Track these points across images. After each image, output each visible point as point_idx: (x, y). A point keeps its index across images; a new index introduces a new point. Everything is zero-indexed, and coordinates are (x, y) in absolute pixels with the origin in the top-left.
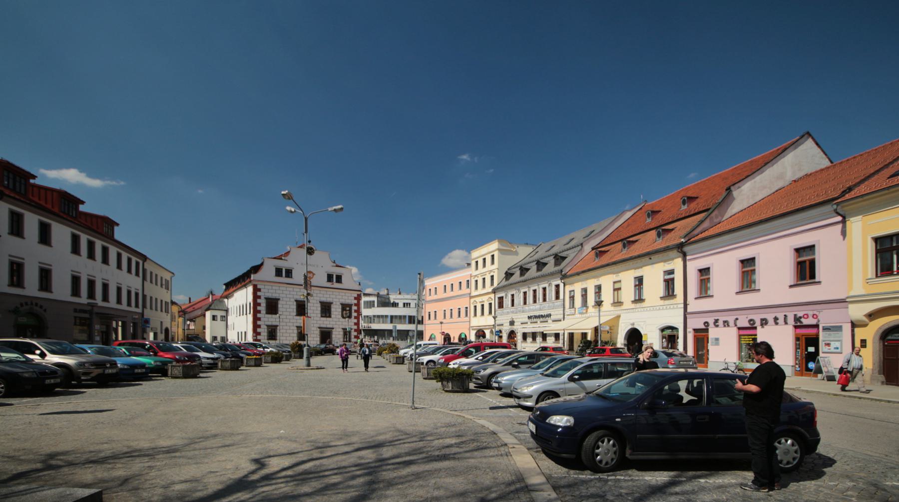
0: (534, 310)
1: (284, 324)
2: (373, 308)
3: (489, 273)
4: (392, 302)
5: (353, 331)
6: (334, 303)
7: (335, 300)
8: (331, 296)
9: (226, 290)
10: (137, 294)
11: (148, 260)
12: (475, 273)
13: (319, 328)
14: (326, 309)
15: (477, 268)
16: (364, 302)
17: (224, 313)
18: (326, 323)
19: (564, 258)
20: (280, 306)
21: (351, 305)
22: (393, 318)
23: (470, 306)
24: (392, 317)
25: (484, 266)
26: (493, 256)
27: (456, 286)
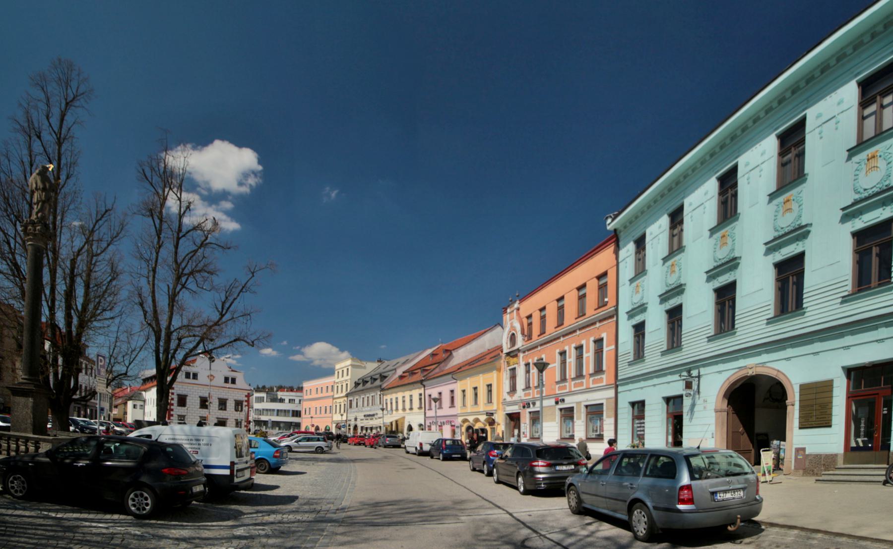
2: (262, 403)
7: (230, 397)
9: (142, 384)
14: (223, 404)
16: (256, 398)
17: (142, 403)
19: (385, 377)
22: (279, 412)
24: (278, 411)
25: (343, 376)
26: (348, 369)
27: (325, 389)
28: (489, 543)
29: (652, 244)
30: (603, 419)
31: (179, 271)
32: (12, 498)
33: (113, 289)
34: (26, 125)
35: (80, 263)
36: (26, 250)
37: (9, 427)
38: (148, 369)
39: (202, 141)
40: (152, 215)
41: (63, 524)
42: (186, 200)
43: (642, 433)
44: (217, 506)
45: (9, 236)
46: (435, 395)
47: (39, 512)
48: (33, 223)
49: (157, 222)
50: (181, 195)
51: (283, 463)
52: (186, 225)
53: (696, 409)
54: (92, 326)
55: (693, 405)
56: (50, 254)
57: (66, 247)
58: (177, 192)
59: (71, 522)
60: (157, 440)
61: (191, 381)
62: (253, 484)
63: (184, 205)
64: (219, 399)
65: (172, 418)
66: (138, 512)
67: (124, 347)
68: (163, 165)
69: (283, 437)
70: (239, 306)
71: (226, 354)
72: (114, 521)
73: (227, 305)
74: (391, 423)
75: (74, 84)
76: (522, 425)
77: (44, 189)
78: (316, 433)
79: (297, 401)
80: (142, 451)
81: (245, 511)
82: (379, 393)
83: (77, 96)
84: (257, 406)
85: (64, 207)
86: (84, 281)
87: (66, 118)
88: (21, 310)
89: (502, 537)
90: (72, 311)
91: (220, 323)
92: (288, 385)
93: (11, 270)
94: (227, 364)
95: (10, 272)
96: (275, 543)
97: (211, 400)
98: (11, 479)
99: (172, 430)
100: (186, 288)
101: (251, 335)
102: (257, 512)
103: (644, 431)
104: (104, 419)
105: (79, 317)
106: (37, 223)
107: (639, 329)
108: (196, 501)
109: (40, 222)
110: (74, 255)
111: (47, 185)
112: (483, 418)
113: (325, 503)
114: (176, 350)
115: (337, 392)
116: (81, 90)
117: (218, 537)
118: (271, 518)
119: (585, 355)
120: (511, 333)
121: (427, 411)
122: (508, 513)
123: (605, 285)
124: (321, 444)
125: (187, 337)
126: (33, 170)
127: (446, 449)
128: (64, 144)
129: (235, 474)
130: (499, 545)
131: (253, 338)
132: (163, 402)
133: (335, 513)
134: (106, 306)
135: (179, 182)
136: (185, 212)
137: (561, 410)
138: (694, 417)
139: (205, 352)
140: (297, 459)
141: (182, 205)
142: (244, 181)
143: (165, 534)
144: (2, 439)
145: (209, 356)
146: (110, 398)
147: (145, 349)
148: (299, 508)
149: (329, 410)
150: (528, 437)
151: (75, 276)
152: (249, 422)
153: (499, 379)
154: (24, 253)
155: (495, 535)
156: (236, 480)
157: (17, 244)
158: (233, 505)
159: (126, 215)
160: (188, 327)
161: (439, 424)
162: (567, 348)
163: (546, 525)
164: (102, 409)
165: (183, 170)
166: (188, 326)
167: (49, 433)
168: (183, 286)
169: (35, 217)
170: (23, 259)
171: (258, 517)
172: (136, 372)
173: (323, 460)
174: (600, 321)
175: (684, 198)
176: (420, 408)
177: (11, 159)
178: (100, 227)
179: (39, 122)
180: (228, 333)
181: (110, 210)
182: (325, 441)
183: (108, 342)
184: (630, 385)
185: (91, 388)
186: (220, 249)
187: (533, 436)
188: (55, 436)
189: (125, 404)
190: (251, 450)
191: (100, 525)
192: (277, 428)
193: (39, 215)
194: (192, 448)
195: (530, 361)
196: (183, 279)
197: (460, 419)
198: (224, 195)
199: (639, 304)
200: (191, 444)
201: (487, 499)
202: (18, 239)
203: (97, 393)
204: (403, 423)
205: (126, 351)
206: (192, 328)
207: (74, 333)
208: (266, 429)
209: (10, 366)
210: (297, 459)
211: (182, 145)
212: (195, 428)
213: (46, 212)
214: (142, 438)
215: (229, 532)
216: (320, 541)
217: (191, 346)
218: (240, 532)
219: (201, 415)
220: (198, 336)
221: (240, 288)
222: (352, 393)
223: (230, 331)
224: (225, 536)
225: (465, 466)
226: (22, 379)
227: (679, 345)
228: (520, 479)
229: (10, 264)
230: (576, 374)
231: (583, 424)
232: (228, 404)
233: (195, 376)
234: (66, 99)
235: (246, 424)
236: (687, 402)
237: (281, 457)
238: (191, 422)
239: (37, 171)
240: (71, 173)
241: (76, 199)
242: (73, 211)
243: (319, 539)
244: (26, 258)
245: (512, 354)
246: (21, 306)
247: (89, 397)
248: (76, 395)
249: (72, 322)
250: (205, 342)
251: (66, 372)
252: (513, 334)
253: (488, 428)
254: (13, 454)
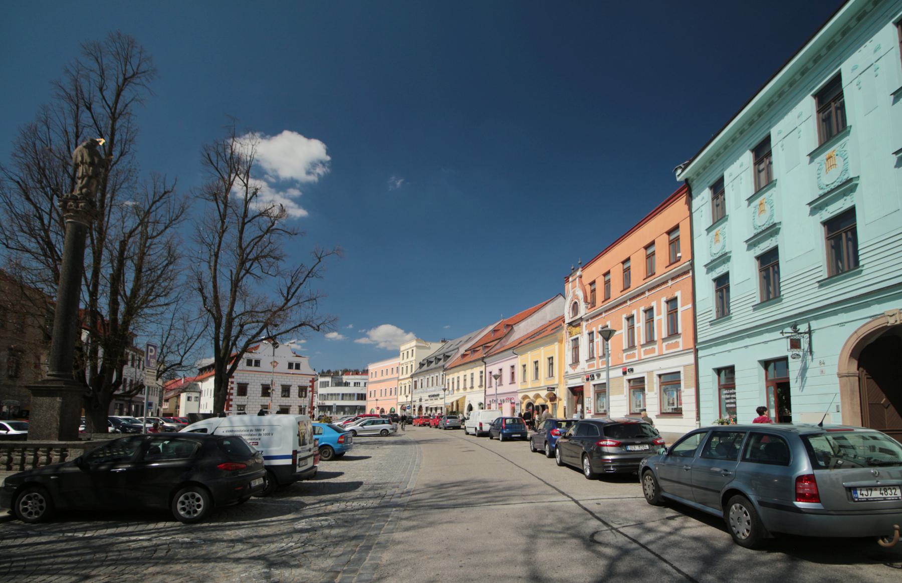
0: (432, 391)
1: (251, 403)
2: (327, 388)
4: (344, 382)
8: (291, 380)
9: (199, 374)
12: (402, 362)
14: (286, 391)
16: (321, 382)
17: (197, 395)
19: (448, 357)
20: (248, 389)
21: (307, 387)
22: (344, 396)
24: (343, 395)
25: (408, 358)
28: (554, 535)
29: (732, 186)
30: (680, 390)
31: (243, 256)
32: (23, 523)
33: (169, 273)
34: (73, 93)
35: (132, 245)
36: (64, 228)
37: (25, 434)
38: (205, 358)
39: (271, 130)
40: (216, 200)
41: (94, 544)
42: (253, 186)
43: (733, 405)
44: (278, 500)
45: (42, 210)
46: (496, 372)
47: (61, 535)
48: (75, 199)
49: (222, 206)
50: (247, 181)
51: (347, 449)
52: (252, 211)
53: (808, 374)
54: (142, 313)
55: (804, 370)
56: (95, 235)
57: (115, 227)
58: (244, 178)
59: (104, 540)
60: (213, 433)
61: (253, 368)
62: (316, 472)
63: (251, 191)
64: (282, 385)
65: (230, 408)
66: (187, 516)
67: (180, 335)
68: (230, 152)
69: (348, 421)
70: (305, 291)
71: (291, 339)
72: (159, 531)
73: (293, 290)
74: (452, 403)
75: (135, 61)
76: (586, 400)
77: (92, 164)
78: (381, 416)
79: (362, 384)
80: (195, 447)
81: (306, 502)
82: (442, 373)
83: (137, 73)
84: (321, 391)
85: (116, 186)
86: (135, 265)
87: (123, 93)
88: (52, 295)
89: (568, 529)
90: (119, 297)
91: (285, 308)
92: (353, 369)
93: (43, 249)
94: (291, 349)
95: (40, 251)
96: (338, 534)
97: (274, 388)
98: (24, 499)
99: (231, 422)
100: (250, 273)
101: (317, 319)
102: (320, 502)
103: (735, 403)
104: (152, 415)
105: (127, 304)
106: (80, 199)
107: (722, 283)
108: (255, 496)
109: (84, 198)
110: (124, 237)
111: (96, 160)
112: (544, 393)
113: (390, 488)
114: (237, 337)
116: (142, 68)
117: (278, 532)
118: (335, 507)
119: (656, 318)
120: (573, 302)
121: (487, 389)
122: (573, 500)
123: (678, 239)
124: (387, 426)
125: (250, 323)
126: (79, 142)
127: (506, 428)
128: (119, 120)
129: (297, 463)
130: (565, 538)
131: (319, 322)
132: (221, 392)
133: (400, 497)
134: (160, 291)
135: (246, 168)
136: (251, 198)
137: (629, 381)
138: (806, 385)
139: (268, 338)
140: (361, 443)
141: (248, 191)
142: (312, 170)
143: (218, 537)
144: (14, 451)
145: (272, 342)
146: (160, 392)
147: (203, 337)
148: (363, 495)
149: (393, 392)
150: (593, 413)
151: (124, 259)
152: (313, 408)
153: (561, 351)
154: (61, 231)
155: (560, 526)
156: (299, 470)
157: (52, 221)
158: (295, 496)
159: (188, 198)
160: (251, 313)
161: (499, 402)
162: (634, 312)
163: (618, 517)
164: (150, 404)
165: (251, 157)
166: (251, 311)
167: (81, 437)
168: (247, 271)
169: (78, 192)
170: (59, 237)
171: (321, 507)
172: (193, 362)
173: (388, 443)
174: (673, 279)
175: (770, 127)
176: (481, 386)
177: (51, 127)
178: (157, 209)
179: (90, 93)
180: (293, 318)
181: (169, 192)
182: (390, 423)
183: (160, 331)
184: (714, 348)
185: (138, 382)
186: (288, 235)
187: (598, 411)
188: (89, 439)
189: (178, 396)
190: (315, 437)
191: (141, 538)
192: (342, 413)
193: (84, 190)
194: (251, 439)
195: (594, 329)
196: (248, 265)
197: (520, 396)
198: (292, 183)
199: (720, 254)
200: (251, 435)
201: (550, 483)
202: (54, 215)
203: (144, 387)
204: (463, 403)
205: (182, 339)
206: (255, 314)
207: (120, 322)
208: (330, 414)
209: (32, 360)
210: (361, 443)
211: (250, 133)
212: (256, 418)
213: (93, 188)
214: (196, 433)
215: (289, 527)
216: (385, 527)
217: (254, 332)
218: (302, 524)
219: (263, 404)
220: (262, 322)
221: (307, 273)
222: (417, 374)
223: (295, 316)
224: (286, 531)
225: (526, 446)
226: (48, 375)
227: (777, 295)
228: (586, 461)
229: (41, 242)
230: (629, 345)
231: (656, 396)
233: (257, 363)
234: (124, 75)
235: (310, 410)
236: (794, 367)
237: (345, 442)
238: (251, 412)
239: (84, 144)
240: (126, 150)
241: (130, 178)
242: (126, 190)
243: (384, 526)
244: (63, 237)
245: (574, 324)
246: (52, 290)
247: (134, 392)
248: (119, 390)
249: (118, 309)
250: (269, 328)
251: (107, 365)
252: (576, 303)
253: (549, 404)
254: (28, 467)
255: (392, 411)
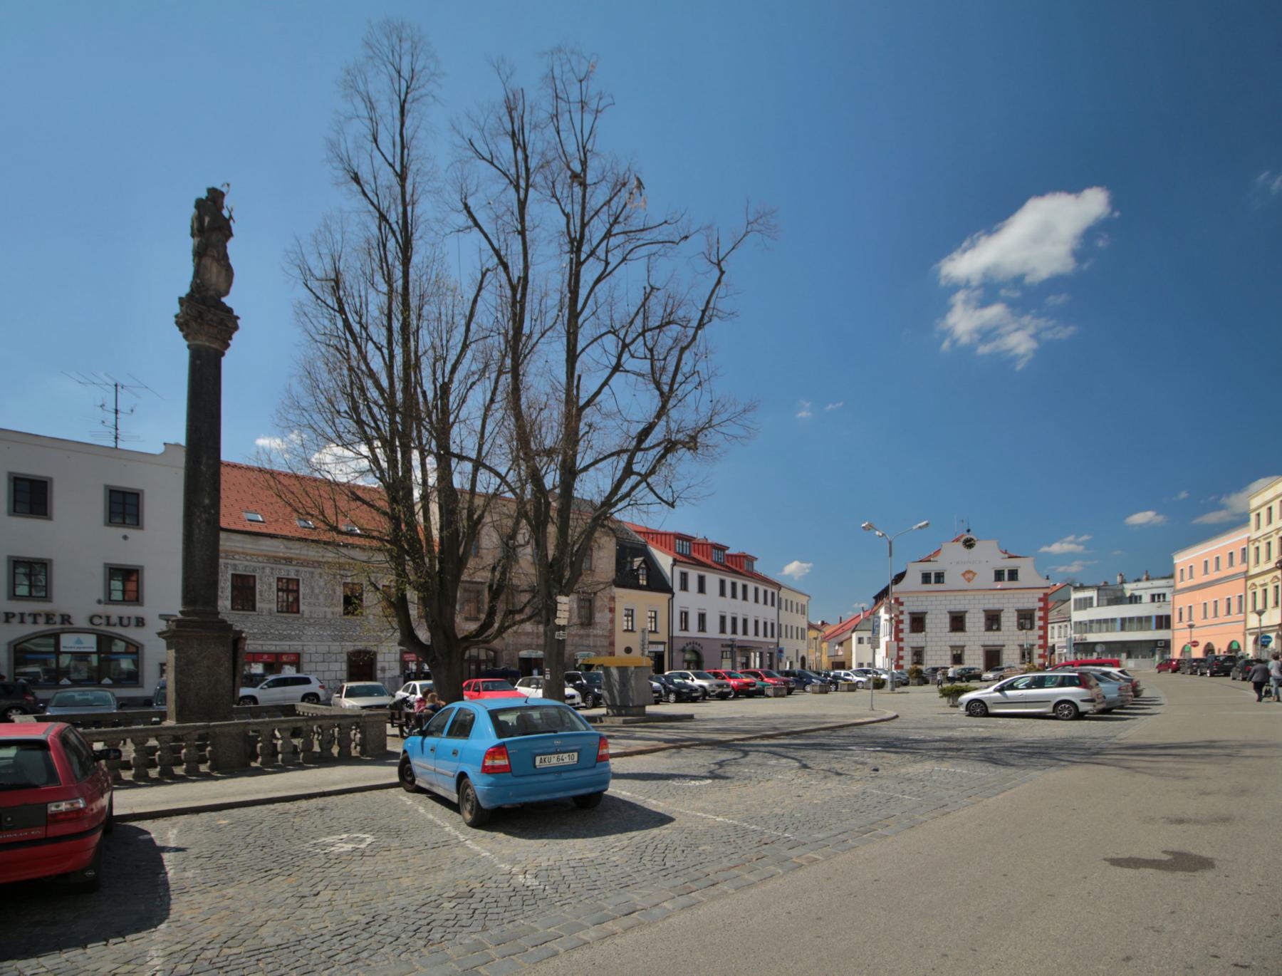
2: (1088, 609)
3: (1277, 534)
4: (1128, 594)
5: (1036, 647)
6: (1006, 610)
10: (772, 625)
11: (782, 589)
12: (1255, 535)
13: (983, 646)
14: (993, 620)
15: (1258, 527)
18: (993, 638)
20: (927, 621)
22: (1125, 623)
23: (1246, 594)
24: (1123, 620)
25: (1270, 521)
27: (1224, 561)
64: (985, 611)
84: (1078, 616)
115: (1257, 561)
232: (1003, 619)
233: (940, 577)
255: (1233, 649)
